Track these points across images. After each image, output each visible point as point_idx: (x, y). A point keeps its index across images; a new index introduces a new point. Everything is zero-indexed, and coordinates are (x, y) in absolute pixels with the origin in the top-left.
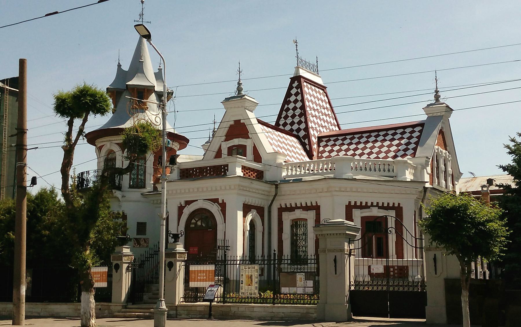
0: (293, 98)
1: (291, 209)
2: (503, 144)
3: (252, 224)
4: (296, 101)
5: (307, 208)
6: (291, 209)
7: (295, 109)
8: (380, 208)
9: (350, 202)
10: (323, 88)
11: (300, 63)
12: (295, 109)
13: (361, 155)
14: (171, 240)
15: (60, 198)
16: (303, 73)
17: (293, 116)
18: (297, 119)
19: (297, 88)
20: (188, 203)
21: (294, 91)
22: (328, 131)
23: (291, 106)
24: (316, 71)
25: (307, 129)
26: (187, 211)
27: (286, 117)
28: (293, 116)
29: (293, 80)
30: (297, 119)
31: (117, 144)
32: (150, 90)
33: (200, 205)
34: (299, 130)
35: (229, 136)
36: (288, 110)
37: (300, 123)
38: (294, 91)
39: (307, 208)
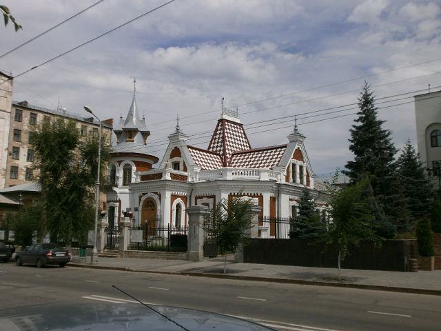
0: (218, 132)
1: (201, 197)
2: (86, 109)
3: (178, 206)
4: (220, 134)
5: (209, 197)
6: (201, 197)
7: (219, 138)
9: (351, 130)
10: (241, 125)
11: (224, 110)
12: (219, 138)
13: (239, 166)
14: (122, 216)
15: (353, 144)
16: (225, 117)
17: (218, 143)
18: (219, 144)
19: (221, 126)
20: (144, 194)
21: (219, 128)
23: (217, 136)
24: (236, 115)
25: (224, 150)
26: (143, 199)
27: (214, 143)
28: (218, 143)
29: (220, 121)
30: (219, 144)
31: (410, 147)
32: (136, 131)
33: (149, 195)
34: (220, 151)
35: (172, 156)
36: (216, 138)
37: (221, 146)
38: (219, 128)
39: (209, 197)
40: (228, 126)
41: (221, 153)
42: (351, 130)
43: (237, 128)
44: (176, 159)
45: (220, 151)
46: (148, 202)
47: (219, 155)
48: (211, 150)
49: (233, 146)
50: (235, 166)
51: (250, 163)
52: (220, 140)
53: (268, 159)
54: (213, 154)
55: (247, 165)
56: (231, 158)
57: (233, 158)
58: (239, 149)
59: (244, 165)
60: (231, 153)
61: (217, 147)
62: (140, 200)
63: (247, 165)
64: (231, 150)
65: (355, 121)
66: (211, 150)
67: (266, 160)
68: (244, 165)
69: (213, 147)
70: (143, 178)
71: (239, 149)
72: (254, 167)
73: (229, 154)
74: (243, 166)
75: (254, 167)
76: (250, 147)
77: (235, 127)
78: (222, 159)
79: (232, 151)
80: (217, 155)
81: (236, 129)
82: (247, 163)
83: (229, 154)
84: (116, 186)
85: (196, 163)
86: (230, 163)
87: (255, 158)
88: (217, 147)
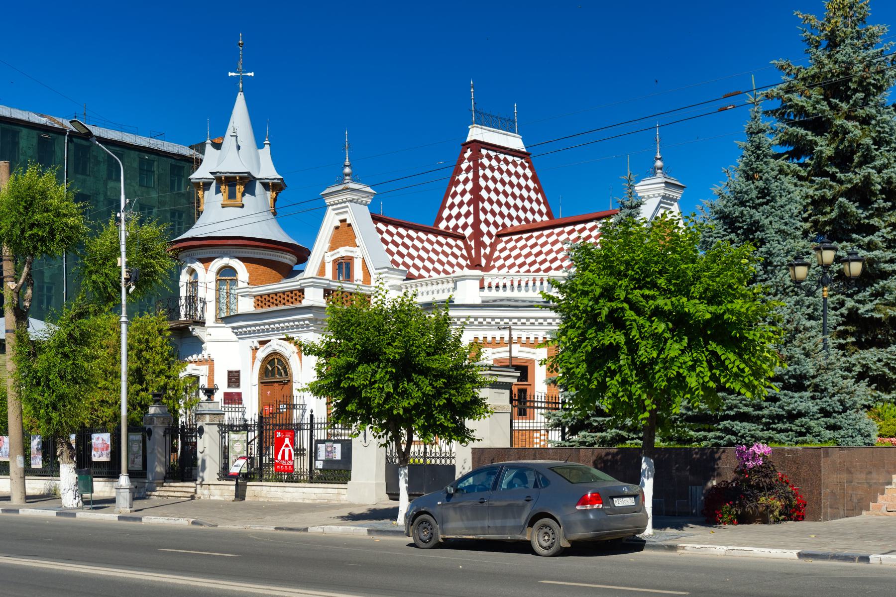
7: (463, 193)
8: (523, 345)
12: (463, 193)
17: (461, 204)
20: (263, 343)
22: (523, 223)
28: (461, 204)
34: (465, 226)
36: (455, 194)
37: (467, 215)
40: (489, 157)
41: (468, 232)
42: (201, 438)
43: (515, 164)
44: (343, 252)
45: (465, 226)
46: (271, 362)
47: (463, 238)
48: (442, 226)
49: (502, 215)
50: (503, 266)
51: (529, 260)
52: (467, 197)
53: (437, 253)
54: (445, 234)
55: (521, 266)
56: (493, 246)
57: (500, 246)
58: (519, 219)
59: (513, 265)
60: (494, 231)
61: (458, 216)
62: (254, 358)
63: (521, 266)
64: (496, 225)
65: (312, 411)
66: (442, 226)
67: (430, 259)
68: (513, 265)
69: (449, 218)
70: (261, 300)
71: (519, 219)
72: (538, 270)
73: (489, 234)
74: (510, 267)
75: (538, 270)
76: (549, 214)
77: (506, 162)
78: (468, 248)
79: (496, 225)
80: (456, 237)
81: (512, 168)
82: (511, 261)
83: (489, 234)
84: (202, 323)
85: (394, 262)
86: (489, 258)
87: (512, 249)
88: (458, 216)
